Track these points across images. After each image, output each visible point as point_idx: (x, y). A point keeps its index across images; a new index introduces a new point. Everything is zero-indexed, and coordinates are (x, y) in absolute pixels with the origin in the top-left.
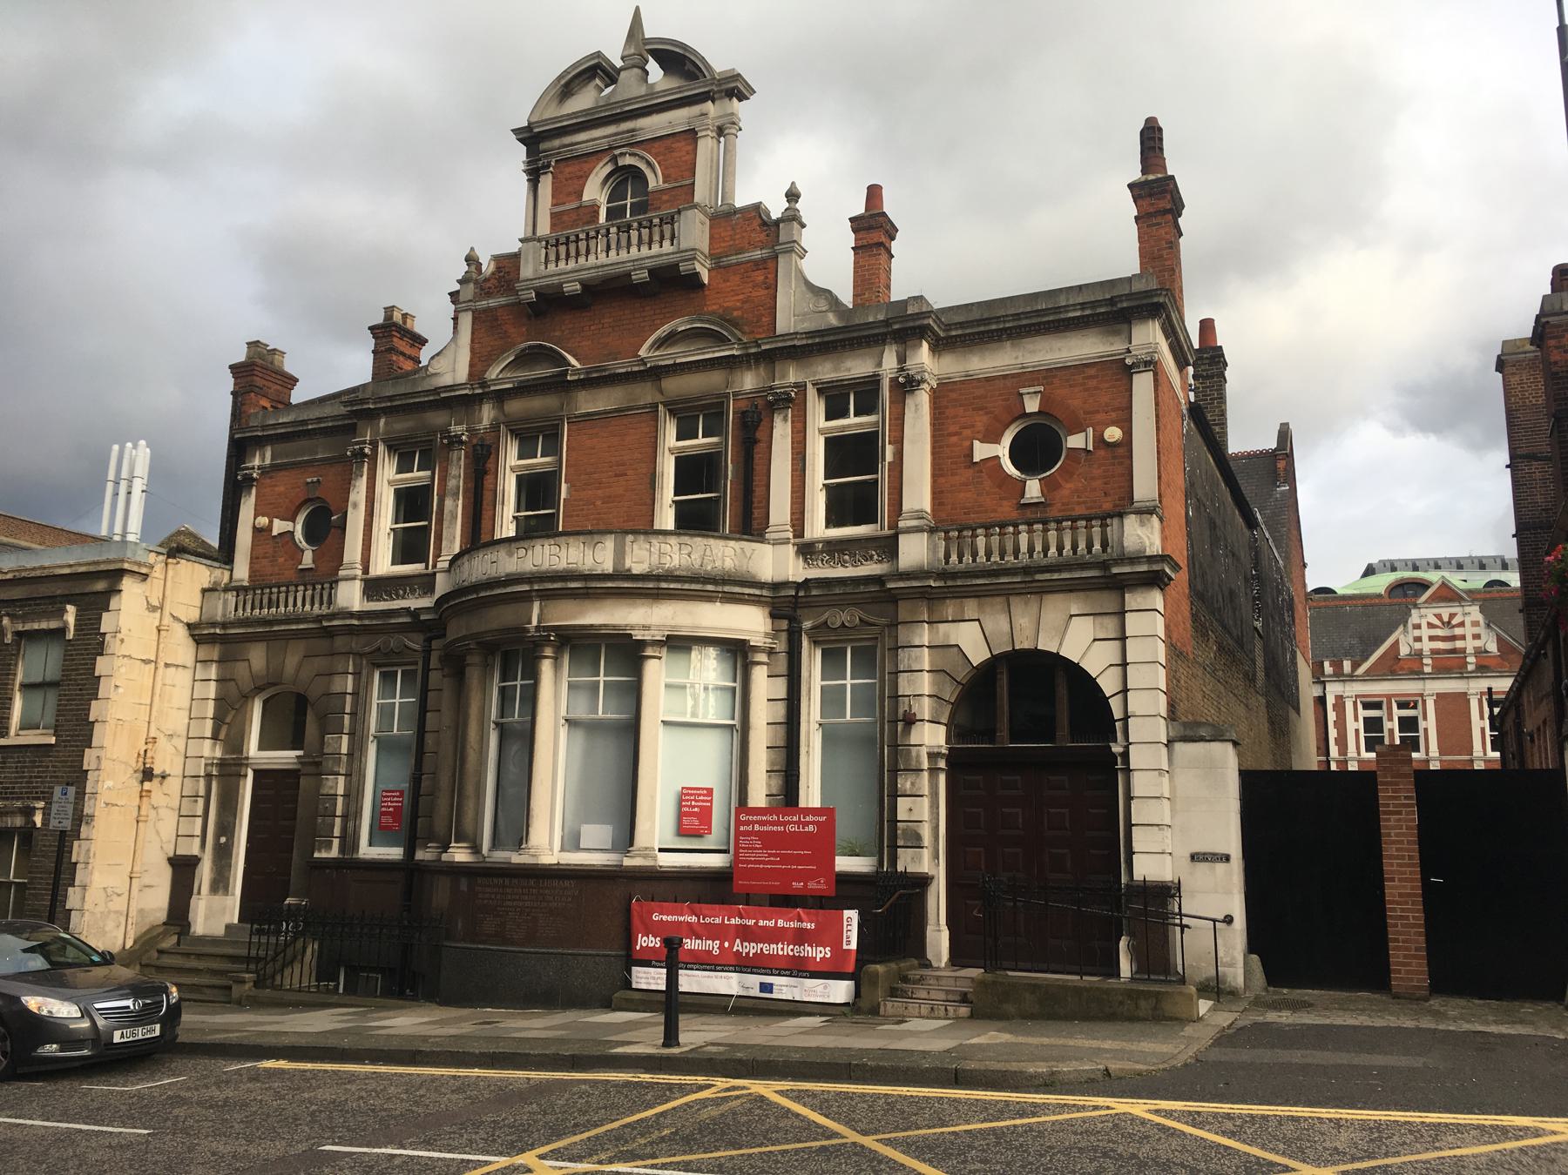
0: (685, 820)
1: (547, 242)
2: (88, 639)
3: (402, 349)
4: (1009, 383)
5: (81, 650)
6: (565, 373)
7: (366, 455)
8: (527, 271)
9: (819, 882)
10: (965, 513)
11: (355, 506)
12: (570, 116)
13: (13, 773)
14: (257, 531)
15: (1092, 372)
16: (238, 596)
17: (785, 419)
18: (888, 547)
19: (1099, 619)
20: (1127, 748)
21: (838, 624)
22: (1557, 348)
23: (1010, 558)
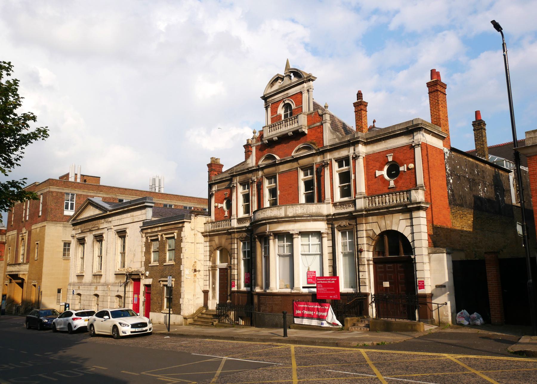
4: (384, 153)
6: (276, 161)
7: (235, 187)
8: (265, 135)
10: (375, 191)
11: (234, 200)
12: (273, 92)
14: (215, 207)
15: (405, 148)
18: (354, 202)
20: (415, 256)
21: (343, 225)
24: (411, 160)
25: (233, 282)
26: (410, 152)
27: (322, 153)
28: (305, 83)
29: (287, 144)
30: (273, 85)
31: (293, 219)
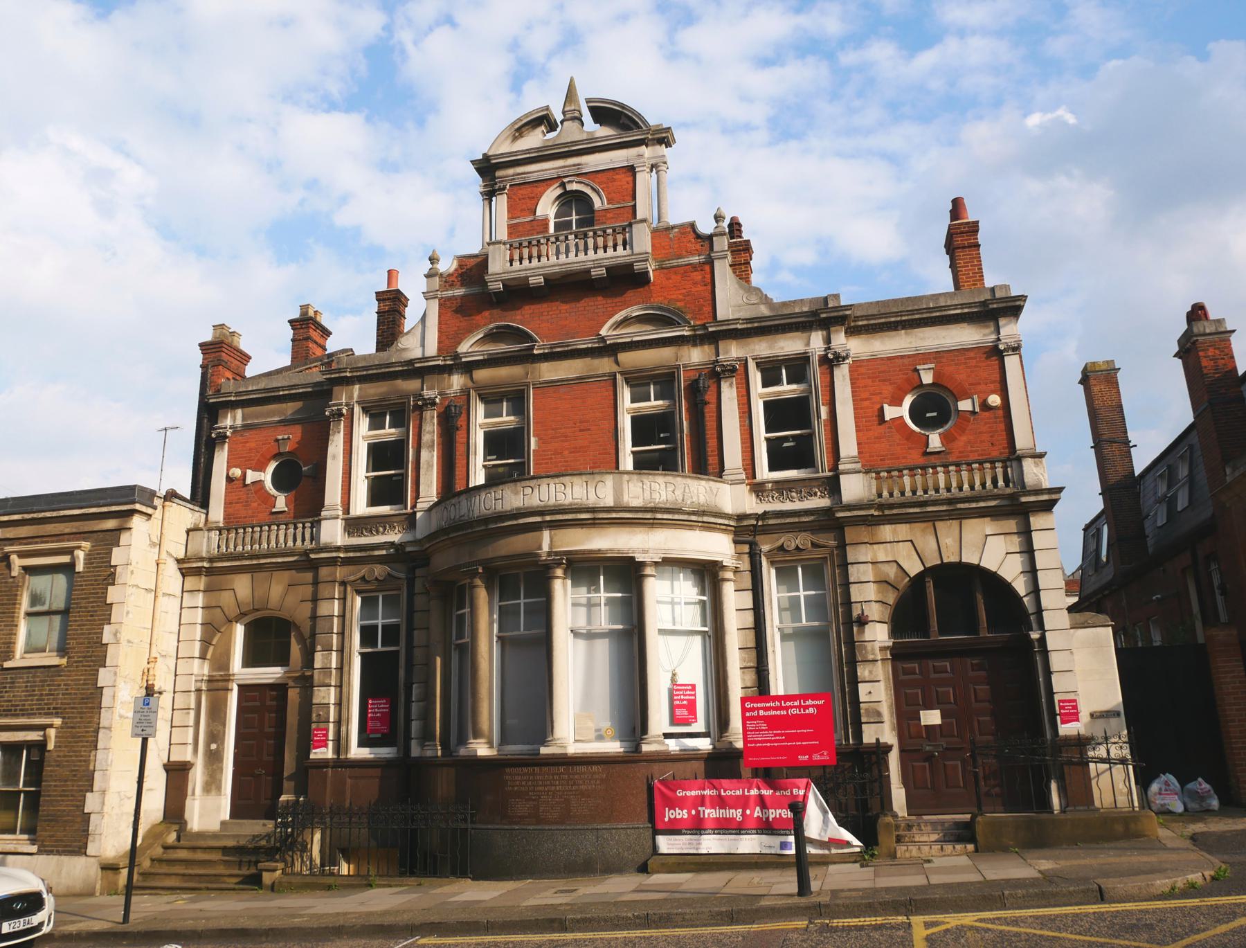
0: (678, 712)
1: (511, 246)
2: (98, 571)
3: (315, 338)
5: (91, 580)
6: (532, 348)
9: (822, 755)
10: (881, 460)
11: (334, 457)
12: (524, 152)
13: (23, 691)
14: (229, 479)
15: (972, 354)
16: (220, 534)
17: (731, 385)
18: (833, 487)
19: (1008, 537)
21: (793, 546)
22: (1205, 357)
23: (931, 492)
24: (992, 386)
25: (317, 729)
26: (988, 366)
27: (714, 337)
28: (644, 146)
29: (573, 305)
30: (521, 136)
31: (649, 516)
